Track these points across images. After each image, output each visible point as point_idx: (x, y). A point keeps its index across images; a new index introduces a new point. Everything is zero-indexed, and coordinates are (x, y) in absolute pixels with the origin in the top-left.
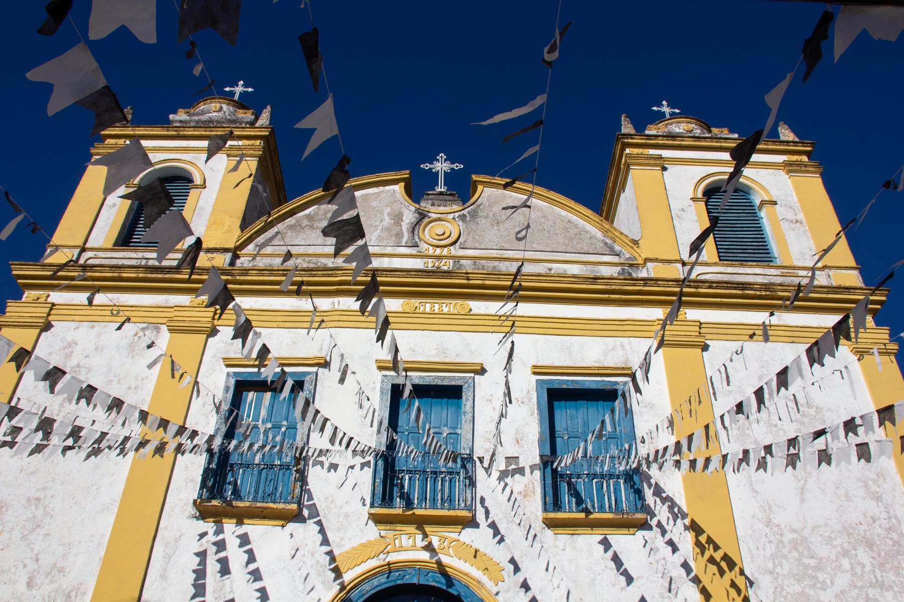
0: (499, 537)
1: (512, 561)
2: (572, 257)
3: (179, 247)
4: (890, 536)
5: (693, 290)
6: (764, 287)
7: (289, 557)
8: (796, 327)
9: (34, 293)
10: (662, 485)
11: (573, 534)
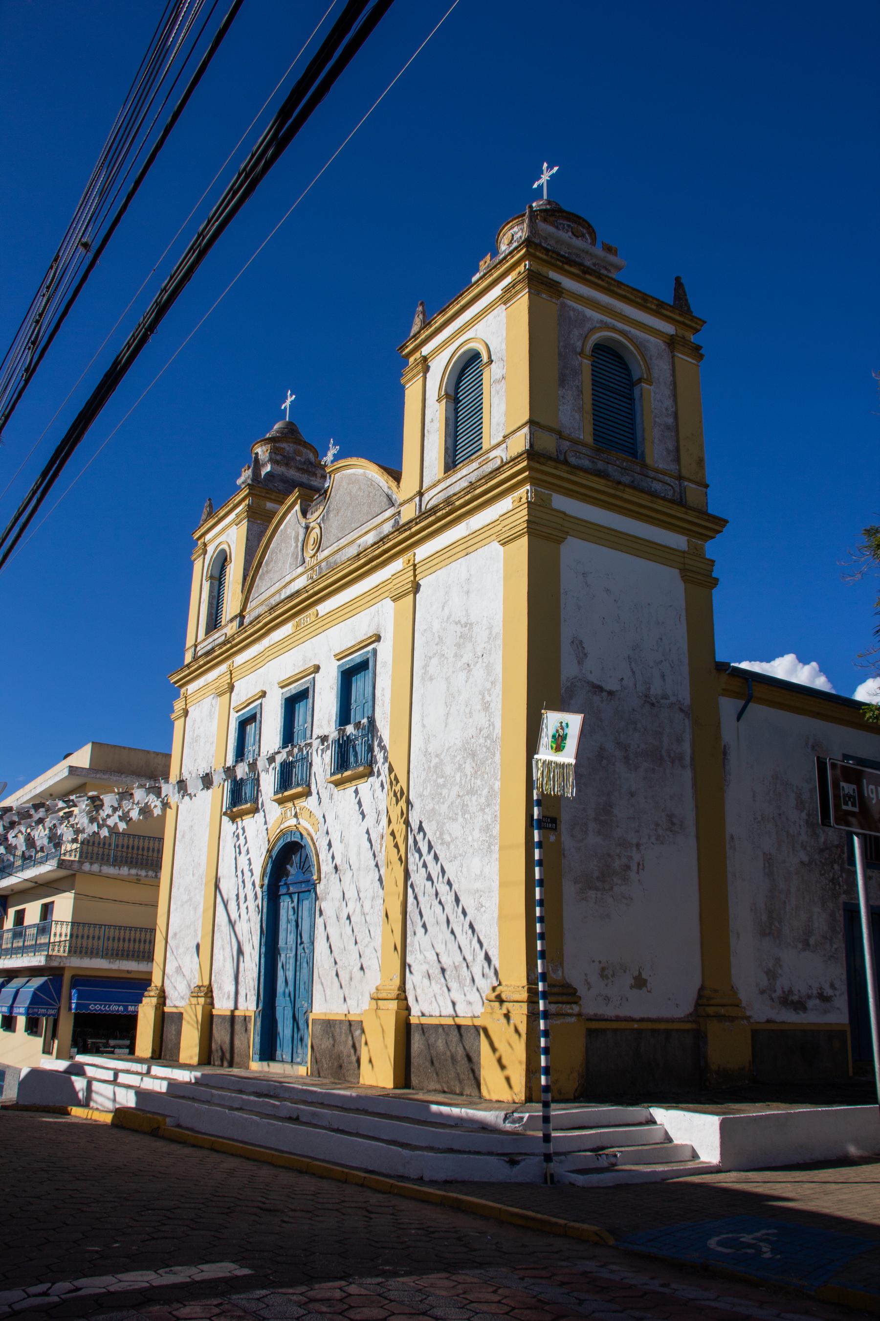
2: (372, 523)
3: (187, 646)
5: (408, 533)
6: (445, 503)
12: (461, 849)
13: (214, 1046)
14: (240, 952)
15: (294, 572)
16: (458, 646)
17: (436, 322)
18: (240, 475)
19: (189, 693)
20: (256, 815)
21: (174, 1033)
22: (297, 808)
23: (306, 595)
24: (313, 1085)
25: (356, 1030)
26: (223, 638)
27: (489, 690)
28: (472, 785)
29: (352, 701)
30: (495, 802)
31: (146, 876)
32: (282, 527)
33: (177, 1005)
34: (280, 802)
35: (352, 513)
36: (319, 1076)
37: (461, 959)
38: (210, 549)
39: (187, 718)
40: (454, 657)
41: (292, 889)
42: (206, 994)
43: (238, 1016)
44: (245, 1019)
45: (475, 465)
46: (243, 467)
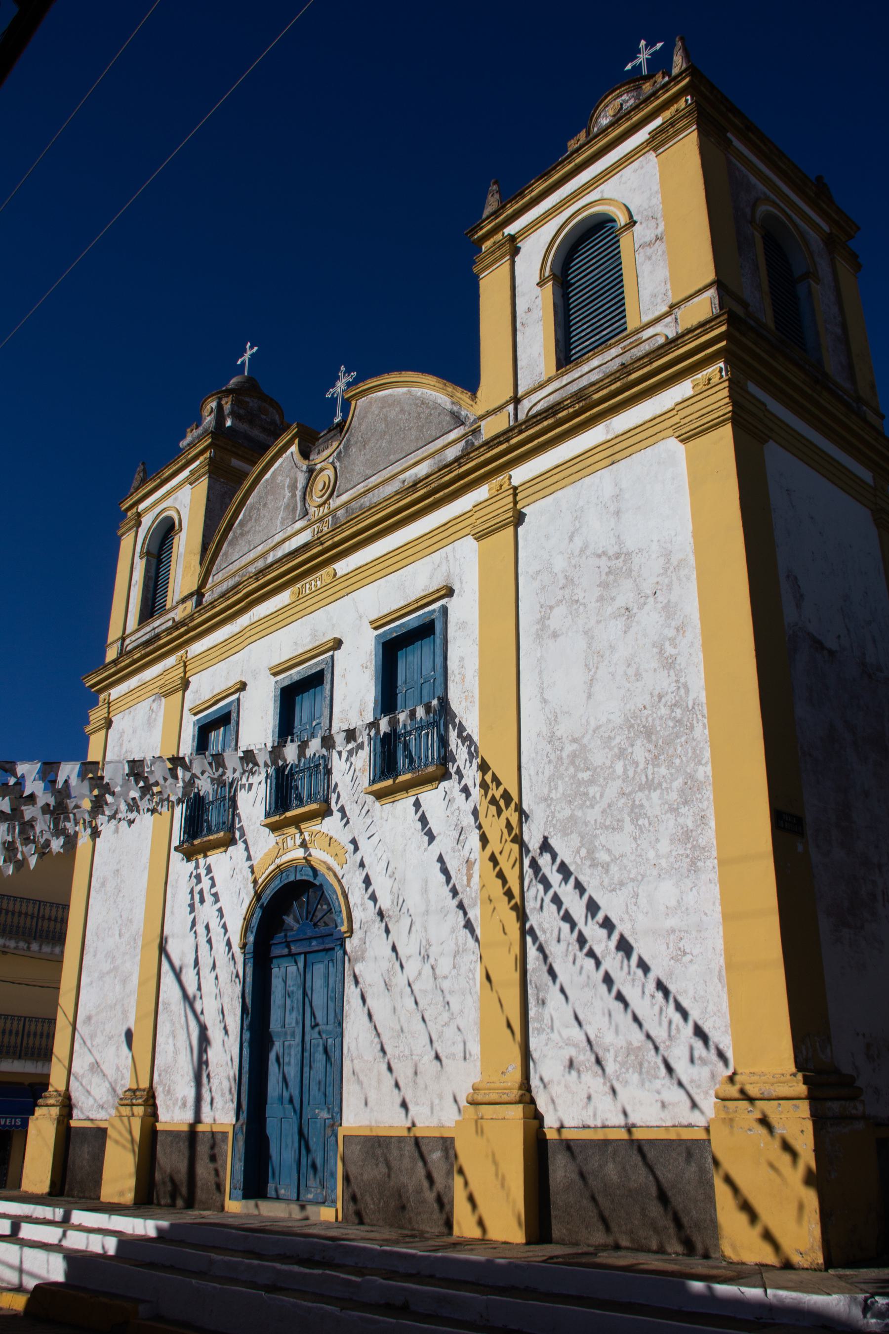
0: (345, 820)
1: (354, 842)
3: (110, 640)
4: (673, 714)
7: (229, 877)
8: (616, 437)
9: (699, 376)
10: (464, 723)
11: (393, 802)
12: (634, 871)
13: (158, 1176)
14: (204, 1040)
15: (289, 528)
16: (604, 585)
17: (532, 191)
18: (184, 436)
19: (112, 698)
20: (231, 849)
21: (87, 1157)
22: (306, 834)
23: (320, 548)
24: (396, 1242)
25: (432, 1151)
26: (170, 623)
27: (672, 640)
28: (650, 777)
29: (399, 683)
30: (699, 796)
31: (16, 948)
32: (268, 476)
33: (91, 1117)
34: (274, 828)
35: (390, 442)
36: (361, 1222)
37: (641, 1037)
38: (147, 521)
39: (110, 731)
40: (597, 601)
41: (294, 949)
42: (146, 1101)
43: (203, 1132)
44: (215, 1138)
45: (614, 352)
46: (189, 427)
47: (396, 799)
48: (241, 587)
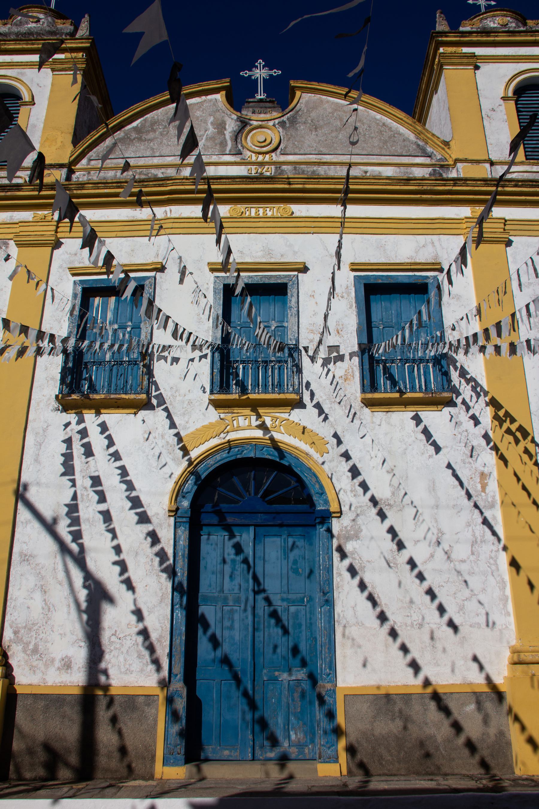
1: (336, 436)
9: (40, 213)
15: (214, 157)
17: (496, 36)
23: (287, 186)
34: (217, 405)
47: (391, 410)
48: (168, 182)
